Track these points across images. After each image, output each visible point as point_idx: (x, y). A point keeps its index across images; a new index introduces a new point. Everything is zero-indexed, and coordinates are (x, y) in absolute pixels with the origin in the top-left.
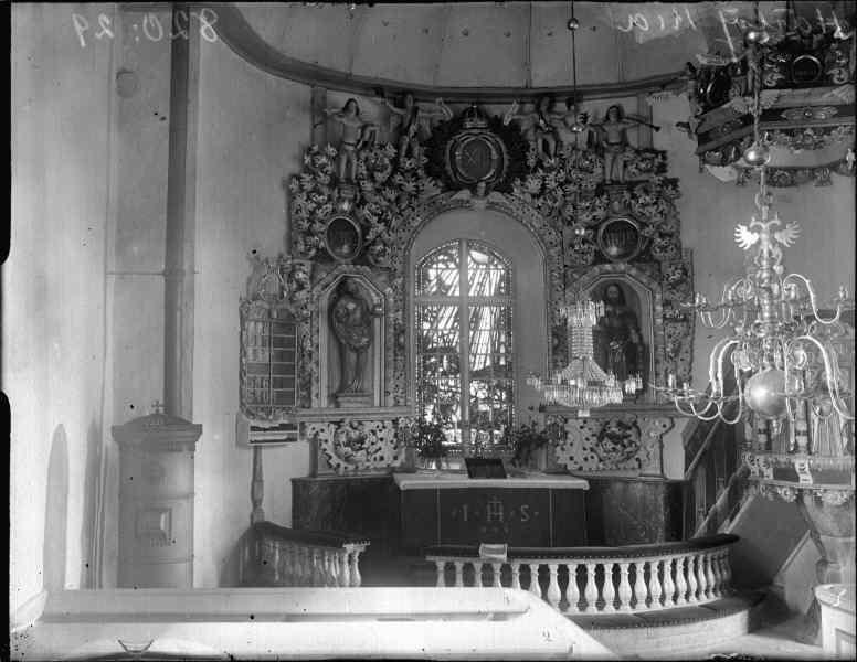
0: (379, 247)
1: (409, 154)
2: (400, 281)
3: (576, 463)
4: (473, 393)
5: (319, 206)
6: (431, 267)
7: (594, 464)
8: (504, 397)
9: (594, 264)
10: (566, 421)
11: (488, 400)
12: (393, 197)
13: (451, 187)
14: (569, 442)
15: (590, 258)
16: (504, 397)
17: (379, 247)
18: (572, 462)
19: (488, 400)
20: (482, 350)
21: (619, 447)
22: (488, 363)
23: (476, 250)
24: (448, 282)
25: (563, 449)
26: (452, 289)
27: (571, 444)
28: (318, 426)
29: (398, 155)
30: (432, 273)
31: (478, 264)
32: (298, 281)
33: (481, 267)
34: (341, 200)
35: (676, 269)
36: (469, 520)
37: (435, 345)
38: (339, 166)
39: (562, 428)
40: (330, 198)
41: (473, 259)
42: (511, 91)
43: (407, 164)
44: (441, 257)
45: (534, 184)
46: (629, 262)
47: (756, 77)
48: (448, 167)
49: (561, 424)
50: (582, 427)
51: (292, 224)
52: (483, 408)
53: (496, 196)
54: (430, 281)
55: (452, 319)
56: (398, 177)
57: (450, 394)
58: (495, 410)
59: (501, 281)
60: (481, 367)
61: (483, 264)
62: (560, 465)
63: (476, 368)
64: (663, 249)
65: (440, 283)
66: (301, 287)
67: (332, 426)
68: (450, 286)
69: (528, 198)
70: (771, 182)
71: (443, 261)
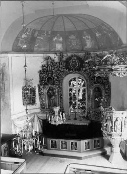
0: (56, 81)
1: (62, 64)
2: (61, 87)
5: (44, 76)
7: (94, 119)
9: (94, 84)
10: (90, 111)
11: (81, 105)
12: (59, 72)
13: (69, 70)
15: (93, 83)
17: (56, 81)
19: (81, 105)
22: (81, 98)
24: (74, 84)
28: (46, 112)
29: (60, 65)
30: (71, 83)
31: (80, 81)
32: (41, 89)
34: (49, 74)
36: (42, 138)
38: (48, 68)
40: (46, 74)
42: (49, 100)
43: (61, 66)
45: (84, 69)
48: (69, 66)
51: (40, 78)
52: (81, 106)
53: (76, 71)
56: (60, 68)
58: (83, 107)
60: (80, 99)
63: (79, 99)
64: (105, 82)
66: (41, 89)
67: (49, 111)
69: (83, 71)
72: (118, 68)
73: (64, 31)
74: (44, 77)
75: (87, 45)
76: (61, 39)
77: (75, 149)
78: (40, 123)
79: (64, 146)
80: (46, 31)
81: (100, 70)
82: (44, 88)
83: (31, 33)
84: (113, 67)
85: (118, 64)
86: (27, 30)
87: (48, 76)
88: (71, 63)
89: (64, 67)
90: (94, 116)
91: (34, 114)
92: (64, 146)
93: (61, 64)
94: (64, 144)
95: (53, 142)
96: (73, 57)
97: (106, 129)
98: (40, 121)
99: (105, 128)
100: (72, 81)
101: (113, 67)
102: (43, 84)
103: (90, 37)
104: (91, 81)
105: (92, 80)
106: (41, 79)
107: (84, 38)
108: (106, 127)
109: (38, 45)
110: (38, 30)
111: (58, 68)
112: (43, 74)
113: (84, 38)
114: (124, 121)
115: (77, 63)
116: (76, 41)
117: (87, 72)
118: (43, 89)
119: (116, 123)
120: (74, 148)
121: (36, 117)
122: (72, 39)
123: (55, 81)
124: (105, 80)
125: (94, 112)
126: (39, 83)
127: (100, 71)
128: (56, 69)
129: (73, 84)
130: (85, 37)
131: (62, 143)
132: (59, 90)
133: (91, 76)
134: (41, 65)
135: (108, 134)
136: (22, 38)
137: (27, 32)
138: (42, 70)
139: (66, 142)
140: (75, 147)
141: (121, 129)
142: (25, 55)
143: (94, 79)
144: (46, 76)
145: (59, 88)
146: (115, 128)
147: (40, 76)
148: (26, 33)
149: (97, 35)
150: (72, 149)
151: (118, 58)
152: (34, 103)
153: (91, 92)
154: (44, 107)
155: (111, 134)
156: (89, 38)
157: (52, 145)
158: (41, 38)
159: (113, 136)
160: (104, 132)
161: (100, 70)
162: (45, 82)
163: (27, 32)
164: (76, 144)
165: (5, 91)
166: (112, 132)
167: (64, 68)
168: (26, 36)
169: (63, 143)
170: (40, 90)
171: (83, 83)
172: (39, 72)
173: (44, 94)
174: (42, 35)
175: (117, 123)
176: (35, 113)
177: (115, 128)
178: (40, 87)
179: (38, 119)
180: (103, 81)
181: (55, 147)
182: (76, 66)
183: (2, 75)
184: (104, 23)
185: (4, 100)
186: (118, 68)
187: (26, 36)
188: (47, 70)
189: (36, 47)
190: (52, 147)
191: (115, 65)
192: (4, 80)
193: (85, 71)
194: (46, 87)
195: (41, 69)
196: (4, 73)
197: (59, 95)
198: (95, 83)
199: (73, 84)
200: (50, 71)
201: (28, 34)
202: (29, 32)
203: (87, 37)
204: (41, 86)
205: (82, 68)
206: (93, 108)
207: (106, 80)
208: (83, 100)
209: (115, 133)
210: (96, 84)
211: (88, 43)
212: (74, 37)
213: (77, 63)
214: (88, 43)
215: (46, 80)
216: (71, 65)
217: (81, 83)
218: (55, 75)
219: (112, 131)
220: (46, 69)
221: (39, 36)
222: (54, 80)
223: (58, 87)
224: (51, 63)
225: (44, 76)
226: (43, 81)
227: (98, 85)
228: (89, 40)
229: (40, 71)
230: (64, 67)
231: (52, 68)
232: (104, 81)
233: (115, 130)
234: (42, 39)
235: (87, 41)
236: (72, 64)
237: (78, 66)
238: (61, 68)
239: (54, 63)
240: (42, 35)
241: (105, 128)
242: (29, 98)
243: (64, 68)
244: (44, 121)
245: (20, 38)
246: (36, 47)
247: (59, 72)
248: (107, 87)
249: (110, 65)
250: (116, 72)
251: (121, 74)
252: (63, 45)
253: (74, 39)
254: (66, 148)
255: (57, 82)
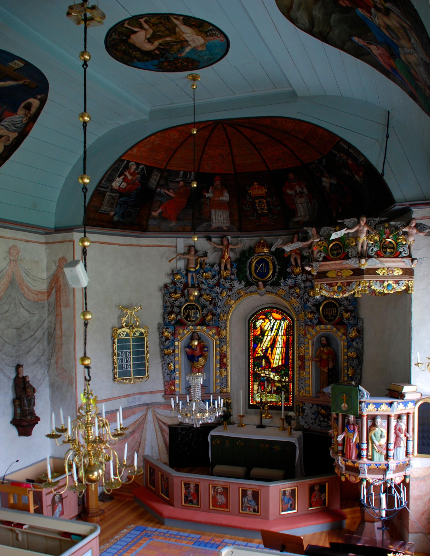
0: (210, 317)
1: (226, 268)
3: (308, 425)
4: (273, 378)
6: (257, 321)
8: (287, 380)
9: (317, 325)
12: (219, 291)
13: (249, 284)
14: (305, 414)
15: (315, 322)
16: (287, 380)
17: (210, 317)
18: (306, 424)
19: (280, 381)
20: (277, 357)
21: (326, 420)
22: (280, 363)
23: (274, 313)
25: (302, 418)
26: (267, 332)
27: (306, 415)
29: (220, 269)
30: (258, 324)
33: (277, 321)
35: (353, 330)
37: (259, 355)
39: (302, 407)
41: (273, 318)
43: (224, 274)
44: (261, 317)
45: (290, 282)
46: (333, 325)
47: (291, 357)
49: (301, 405)
50: (311, 408)
51: (165, 307)
53: (269, 288)
54: (257, 328)
55: (264, 341)
57: (266, 378)
59: (287, 328)
60: (277, 365)
61: (278, 320)
62: (301, 425)
64: (348, 319)
65: (262, 329)
68: (267, 330)
69: (287, 288)
70: (132, 305)
71: (263, 319)
72: (379, 268)
73: (232, 172)
74: (177, 303)
75: (299, 214)
76: (226, 197)
77: (251, 510)
78: (163, 435)
79: (221, 499)
80: (182, 172)
81: (328, 275)
82: (173, 334)
83: (139, 176)
84: (365, 264)
85: (378, 255)
86: (126, 168)
87: (187, 301)
88: (253, 265)
89: (233, 277)
90: (315, 419)
91: (145, 407)
92: (221, 499)
93: (223, 268)
94: (221, 494)
95: (189, 487)
96: (259, 247)
97: (343, 451)
98: (161, 428)
99: (340, 448)
100: (258, 319)
101: (365, 264)
102: (173, 322)
103: (305, 190)
104: (310, 316)
105: (311, 312)
106: (168, 309)
107: (289, 192)
108: (343, 445)
109: (160, 214)
110: (159, 170)
111: (217, 277)
112: (173, 296)
113: (289, 192)
114: (395, 429)
115: (271, 266)
116: (268, 202)
117: (297, 291)
118: (171, 338)
119: (372, 434)
120: (249, 508)
121: (150, 418)
122: (256, 197)
123: (207, 315)
124: (347, 311)
125: (315, 407)
126: (161, 321)
127: (328, 277)
128: (211, 282)
129: (261, 328)
130: (291, 190)
131: (214, 491)
132: (218, 342)
133: (308, 300)
134: (168, 267)
135: (348, 468)
136: (113, 190)
137: (127, 174)
138: (172, 284)
139: (226, 490)
140: (253, 503)
141: (385, 452)
142: (411, 533)
143: (318, 309)
144: (182, 300)
145: (216, 337)
146: (367, 449)
147: (165, 301)
148: (126, 176)
149: (324, 184)
150: (242, 510)
151: (377, 238)
152: (141, 370)
153: (308, 348)
154: (174, 390)
155: (356, 465)
156: (304, 192)
157: (186, 497)
158: (167, 192)
159: (361, 471)
160: (340, 461)
161: (328, 275)
162: (179, 317)
163: (127, 174)
164: (256, 495)
165: (61, 337)
166: (360, 461)
167: (232, 280)
168: (124, 185)
169: (219, 490)
170: (164, 339)
171: (284, 326)
172: (161, 290)
173: (174, 351)
174: (171, 185)
175: (375, 435)
176: (148, 405)
177: (367, 449)
178: (162, 333)
179: (158, 427)
180: (342, 316)
181: (195, 501)
182: (268, 273)
183: (56, 292)
184: (341, 143)
185: (60, 362)
186: (379, 268)
187: (124, 185)
188: (186, 285)
189: (155, 218)
190: (186, 501)
191: (370, 257)
192: (60, 306)
193: (291, 287)
194: (181, 332)
195: (168, 280)
196: (60, 286)
197: (218, 356)
198: (320, 323)
199: (261, 328)
200: (193, 286)
201: (129, 177)
202: (131, 174)
203: (298, 189)
204: (167, 328)
205: (285, 280)
206: (314, 395)
207: (351, 312)
208: (284, 369)
209: (370, 462)
210: (322, 326)
211: (300, 206)
212: (263, 191)
213: (271, 266)
214: (300, 206)
215: (180, 312)
216: (253, 268)
217: (279, 326)
218: (206, 297)
219: (359, 456)
220: (183, 280)
221: (162, 186)
222: (205, 312)
223: (215, 334)
224: (196, 265)
225: (176, 299)
226: (173, 316)
227: (329, 327)
228: (303, 200)
229: (166, 286)
230: (233, 277)
231: (201, 279)
232: (346, 315)
233: (370, 453)
234: (172, 195)
235: (299, 201)
236: (256, 268)
237: (273, 274)
238: (225, 279)
239: (206, 264)
240: (171, 185)
241: (340, 448)
242: (130, 359)
243: (232, 280)
244: (173, 428)
245: (107, 188)
246: (155, 218)
247: (219, 291)
248: (353, 334)
249: (355, 257)
250: (373, 279)
251: (389, 285)
252: (231, 215)
253: (261, 197)
254: (226, 505)
255: (211, 320)
